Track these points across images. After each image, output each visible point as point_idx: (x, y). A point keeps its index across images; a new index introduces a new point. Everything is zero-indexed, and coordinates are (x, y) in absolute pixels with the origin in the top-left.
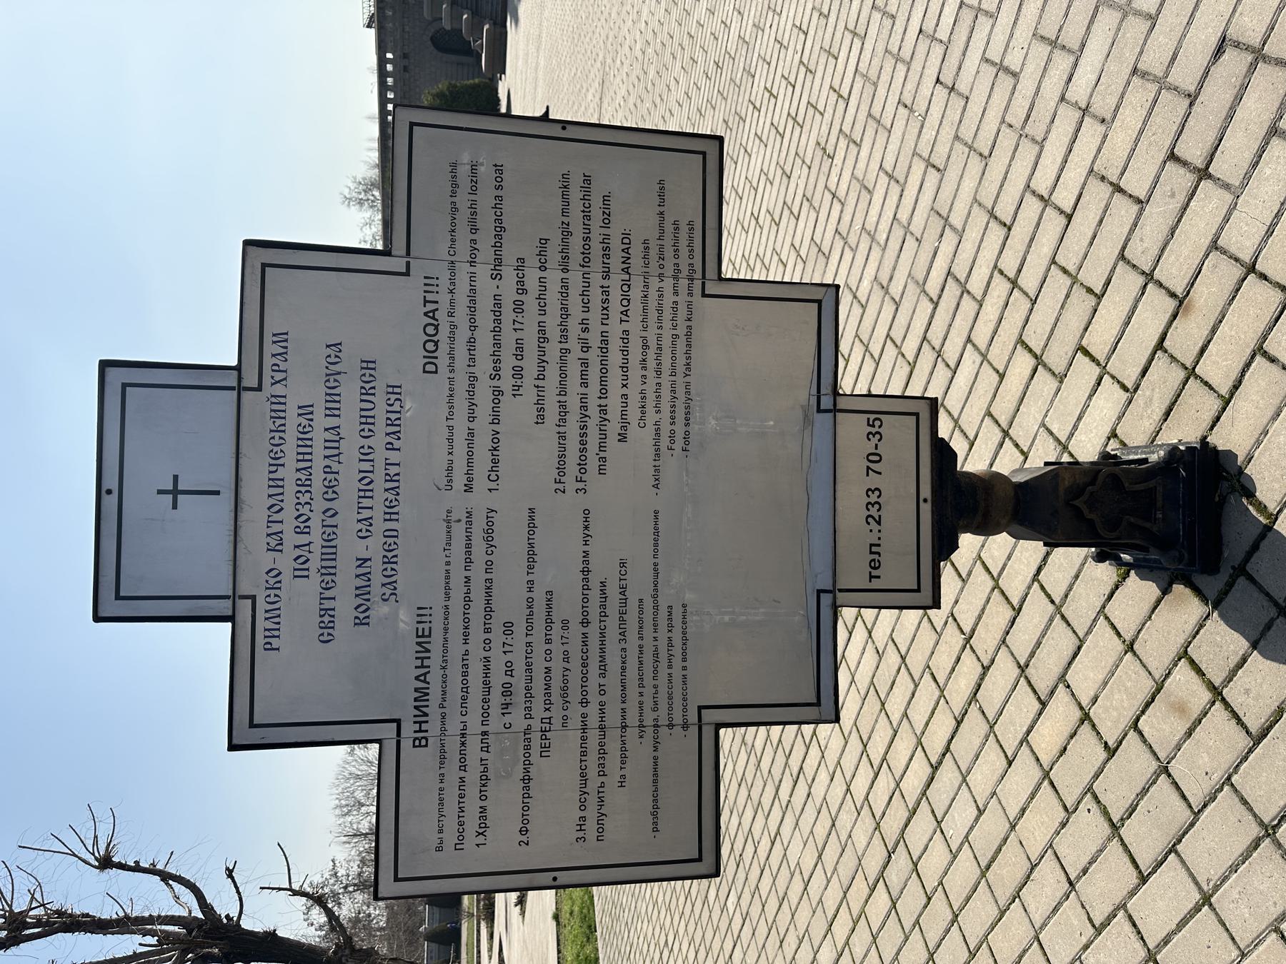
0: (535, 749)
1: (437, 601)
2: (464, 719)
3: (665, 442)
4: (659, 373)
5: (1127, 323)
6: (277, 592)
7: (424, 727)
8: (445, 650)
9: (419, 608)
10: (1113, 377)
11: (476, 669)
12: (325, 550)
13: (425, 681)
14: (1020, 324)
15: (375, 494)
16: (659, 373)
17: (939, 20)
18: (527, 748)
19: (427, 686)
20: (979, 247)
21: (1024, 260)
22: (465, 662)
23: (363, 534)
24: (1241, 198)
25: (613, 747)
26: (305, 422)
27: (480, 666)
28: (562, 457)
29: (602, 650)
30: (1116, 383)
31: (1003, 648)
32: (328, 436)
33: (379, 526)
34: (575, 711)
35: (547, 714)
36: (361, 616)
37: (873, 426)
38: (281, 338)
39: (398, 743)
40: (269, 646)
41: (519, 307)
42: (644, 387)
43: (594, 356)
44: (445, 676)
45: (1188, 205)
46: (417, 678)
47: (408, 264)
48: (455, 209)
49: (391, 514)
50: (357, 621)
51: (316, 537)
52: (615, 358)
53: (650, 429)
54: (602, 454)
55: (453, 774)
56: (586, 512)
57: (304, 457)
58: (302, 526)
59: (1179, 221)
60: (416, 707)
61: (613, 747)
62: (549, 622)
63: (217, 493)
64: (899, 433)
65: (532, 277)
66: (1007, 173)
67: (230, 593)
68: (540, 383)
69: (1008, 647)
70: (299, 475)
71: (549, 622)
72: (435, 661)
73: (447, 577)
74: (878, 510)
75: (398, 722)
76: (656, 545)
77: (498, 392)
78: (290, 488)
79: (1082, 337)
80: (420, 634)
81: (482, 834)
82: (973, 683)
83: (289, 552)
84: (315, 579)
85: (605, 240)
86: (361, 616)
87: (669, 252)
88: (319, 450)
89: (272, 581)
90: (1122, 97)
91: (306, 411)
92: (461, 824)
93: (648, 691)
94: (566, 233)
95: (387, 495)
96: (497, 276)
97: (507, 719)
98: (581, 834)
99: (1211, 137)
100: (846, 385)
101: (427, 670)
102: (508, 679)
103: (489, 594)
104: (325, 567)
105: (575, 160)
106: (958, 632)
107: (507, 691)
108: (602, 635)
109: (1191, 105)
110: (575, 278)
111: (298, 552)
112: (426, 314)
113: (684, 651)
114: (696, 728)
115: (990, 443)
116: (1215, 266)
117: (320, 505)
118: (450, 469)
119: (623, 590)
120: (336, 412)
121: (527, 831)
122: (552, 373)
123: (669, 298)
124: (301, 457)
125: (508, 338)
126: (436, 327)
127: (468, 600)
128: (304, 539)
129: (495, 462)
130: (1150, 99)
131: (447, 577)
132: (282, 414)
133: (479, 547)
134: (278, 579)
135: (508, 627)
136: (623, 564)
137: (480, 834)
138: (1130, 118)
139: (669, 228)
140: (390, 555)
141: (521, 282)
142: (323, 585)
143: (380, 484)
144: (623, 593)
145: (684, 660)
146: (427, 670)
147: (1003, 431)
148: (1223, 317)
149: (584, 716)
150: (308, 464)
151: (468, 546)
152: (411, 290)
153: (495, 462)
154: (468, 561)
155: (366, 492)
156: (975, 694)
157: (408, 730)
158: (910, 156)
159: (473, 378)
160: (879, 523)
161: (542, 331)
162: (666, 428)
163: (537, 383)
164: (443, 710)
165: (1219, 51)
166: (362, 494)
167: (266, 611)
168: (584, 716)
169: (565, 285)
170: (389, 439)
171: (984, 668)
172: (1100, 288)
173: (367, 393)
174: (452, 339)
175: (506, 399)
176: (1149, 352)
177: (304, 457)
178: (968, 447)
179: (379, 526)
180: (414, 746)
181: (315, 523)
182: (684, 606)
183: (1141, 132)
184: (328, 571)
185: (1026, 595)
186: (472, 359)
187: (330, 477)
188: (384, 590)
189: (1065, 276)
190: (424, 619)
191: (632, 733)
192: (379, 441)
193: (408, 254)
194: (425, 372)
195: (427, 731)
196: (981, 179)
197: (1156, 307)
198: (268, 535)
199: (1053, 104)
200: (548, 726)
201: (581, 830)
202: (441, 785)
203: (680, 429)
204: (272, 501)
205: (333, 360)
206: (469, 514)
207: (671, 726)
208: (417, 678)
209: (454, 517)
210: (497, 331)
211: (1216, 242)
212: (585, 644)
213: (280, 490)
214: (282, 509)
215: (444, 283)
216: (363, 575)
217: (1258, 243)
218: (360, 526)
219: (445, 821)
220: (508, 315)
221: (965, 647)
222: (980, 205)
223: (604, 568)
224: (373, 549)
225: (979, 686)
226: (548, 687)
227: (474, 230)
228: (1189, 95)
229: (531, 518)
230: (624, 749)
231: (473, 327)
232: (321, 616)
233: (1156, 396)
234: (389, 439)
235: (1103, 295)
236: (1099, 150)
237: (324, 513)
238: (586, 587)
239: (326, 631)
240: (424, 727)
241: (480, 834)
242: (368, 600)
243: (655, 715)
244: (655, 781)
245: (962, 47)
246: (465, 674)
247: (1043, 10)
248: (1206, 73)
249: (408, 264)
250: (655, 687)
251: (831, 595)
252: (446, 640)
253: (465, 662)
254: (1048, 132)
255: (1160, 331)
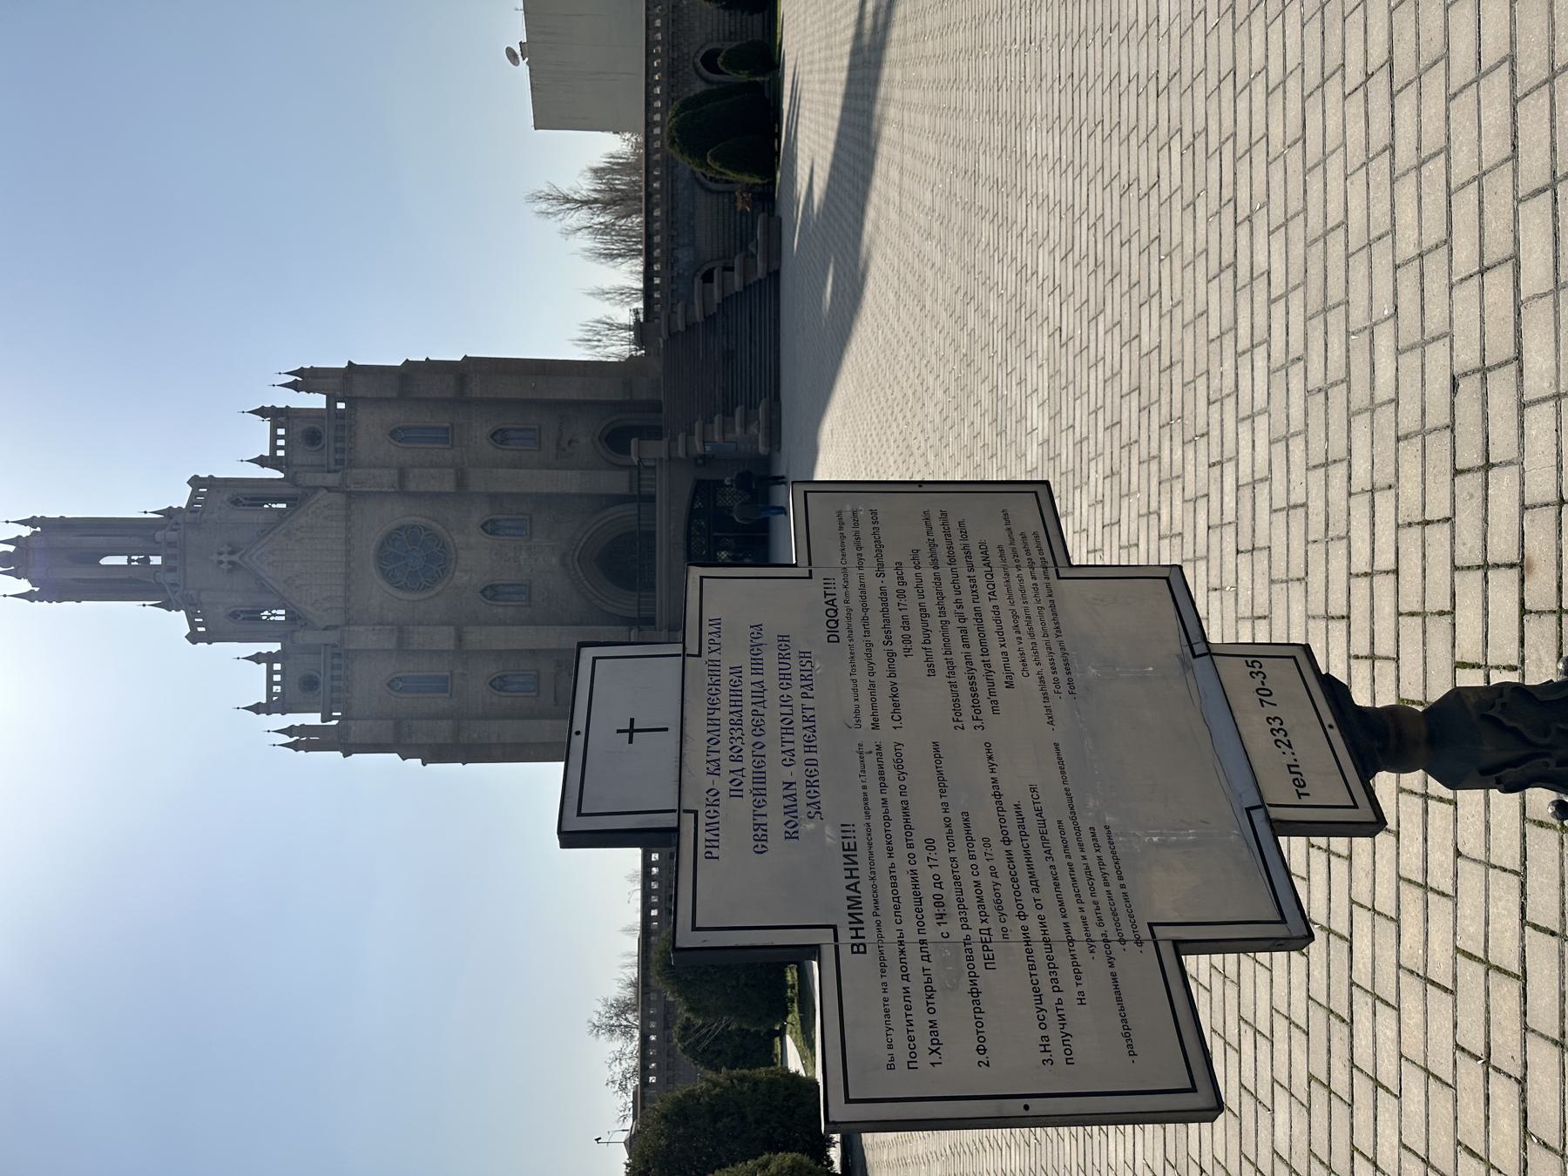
0: (979, 962)
1: (859, 819)
2: (899, 927)
3: (1050, 688)
4: (1032, 635)
5: (1486, 615)
6: (716, 808)
7: (860, 933)
8: (872, 863)
9: (842, 825)
10: (1497, 668)
11: (905, 881)
12: (756, 775)
13: (856, 890)
14: (1393, 686)
15: (795, 732)
16: (1032, 635)
17: (1222, 510)
18: (970, 958)
19: (858, 895)
20: (1327, 651)
21: (1372, 631)
22: (893, 874)
23: (788, 762)
24: (1525, 463)
25: (1063, 961)
26: (735, 679)
27: (908, 879)
28: (956, 701)
29: (1030, 867)
30: (1503, 672)
31: (1529, 1036)
32: (754, 688)
33: (801, 756)
34: (1015, 925)
35: (985, 926)
36: (791, 831)
37: (1253, 667)
38: (716, 622)
39: (837, 948)
40: (709, 855)
41: (901, 594)
42: (1021, 646)
43: (971, 625)
44: (874, 887)
45: (1487, 495)
46: (848, 887)
47: (810, 571)
48: (843, 536)
49: (810, 746)
50: (787, 835)
51: (748, 763)
52: (990, 625)
53: (1034, 678)
54: (993, 698)
55: (896, 985)
56: (988, 746)
57: (736, 703)
58: (736, 755)
59: (1486, 510)
60: (850, 915)
61: (1063, 961)
62: (970, 840)
63: (666, 729)
64: (1281, 675)
65: (909, 574)
66: (1327, 577)
67: (676, 808)
68: (927, 646)
69: (1533, 1031)
70: (732, 716)
71: (970, 840)
72: (863, 871)
73: (866, 799)
74: (1286, 735)
75: (834, 928)
76: (1063, 772)
77: (891, 655)
78: (725, 726)
79: (1453, 655)
80: (846, 847)
81: (935, 1051)
82: (1517, 1114)
83: (726, 776)
84: (748, 799)
85: (966, 549)
86: (791, 831)
87: (1022, 552)
88: (747, 699)
89: (711, 799)
90: (1397, 461)
91: (736, 670)
92: (911, 1039)
93: (1089, 909)
94: (933, 545)
95: (805, 732)
96: (881, 574)
97: (943, 928)
98: (1046, 1056)
99: (1479, 439)
100: (1214, 638)
101: (856, 880)
102: (938, 891)
103: (906, 814)
104: (757, 789)
105: (935, 504)
106: (1472, 1062)
107: (939, 902)
108: (1027, 853)
109: (1452, 431)
110: (945, 571)
111: (733, 776)
112: (826, 603)
113: (1118, 870)
114: (1152, 944)
115: (1414, 817)
116: (1532, 521)
117: (749, 739)
118: (857, 711)
119: (1039, 812)
120: (760, 671)
121: (985, 1050)
122: (937, 639)
123: (1028, 582)
124: (733, 703)
125: (896, 615)
126: (836, 611)
127: (887, 819)
128: (738, 766)
129: (896, 706)
130: (1420, 448)
131: (866, 799)
132: (718, 673)
133: (891, 774)
134: (716, 797)
135: (930, 844)
136: (1033, 790)
137: (933, 1051)
138: (1411, 469)
139: (1018, 538)
140: (812, 780)
141: (900, 577)
142: (756, 803)
143: (798, 724)
144: (1040, 815)
145: (1121, 878)
146: (856, 880)
147: (1422, 795)
148: (1561, 551)
149: (1025, 929)
150: (740, 708)
151: (881, 773)
152: (815, 588)
153: (896, 706)
154: (883, 786)
155: (787, 730)
156: (1525, 1126)
157: (845, 936)
158: (1234, 623)
159: (869, 645)
160: (1290, 746)
161: (923, 609)
162: (1049, 677)
163: (924, 646)
164: (878, 918)
165: (1454, 387)
166: (784, 731)
167: (707, 824)
168: (1025, 929)
169: (937, 578)
170: (804, 690)
171: (1519, 1082)
172: (1449, 604)
173: (784, 657)
174: (849, 617)
175: (900, 660)
176: (1517, 623)
177: (736, 703)
178: (1395, 839)
179: (801, 756)
180: (853, 952)
181: (747, 753)
182: (1107, 827)
183: (1424, 473)
184: (759, 792)
185: (1524, 951)
186: (867, 631)
187: (757, 718)
188: (810, 809)
189: (1415, 618)
190: (848, 834)
191: (1081, 948)
192: (795, 691)
193: (810, 564)
194: (829, 641)
195: (863, 937)
196: (1306, 597)
197: (1503, 586)
198: (708, 762)
199: (1344, 503)
200: (988, 937)
201: (1045, 1051)
202: (885, 995)
203: (1062, 675)
204: (710, 736)
205: (756, 635)
206: (879, 747)
207: (1122, 941)
208: (848, 887)
209: (865, 749)
210: (885, 611)
211: (1523, 504)
212: (1010, 860)
213: (717, 728)
214: (719, 742)
215: (839, 581)
216: (790, 796)
217: (1555, 482)
218: (784, 756)
219: (894, 1035)
220: (893, 600)
221: (1487, 1074)
222: (1314, 618)
223: (1014, 792)
224: (797, 773)
225: (1525, 1111)
226: (980, 899)
227: (859, 548)
228: (1448, 427)
229: (936, 750)
230: (1076, 965)
231: (865, 609)
232: (755, 830)
233: (1542, 653)
234: (804, 690)
235: (1454, 609)
236: (1397, 508)
237: (753, 745)
238: (1000, 809)
239: (760, 843)
240: (860, 933)
241: (933, 1051)
242: (796, 817)
243: (1102, 930)
244: (1119, 1000)
245: (1250, 515)
246: (894, 885)
247: (1307, 449)
248: (1453, 404)
249: (810, 571)
250: (1096, 903)
251: (1262, 810)
252: (871, 853)
253: (893, 874)
254: (1349, 524)
255: (1517, 600)
